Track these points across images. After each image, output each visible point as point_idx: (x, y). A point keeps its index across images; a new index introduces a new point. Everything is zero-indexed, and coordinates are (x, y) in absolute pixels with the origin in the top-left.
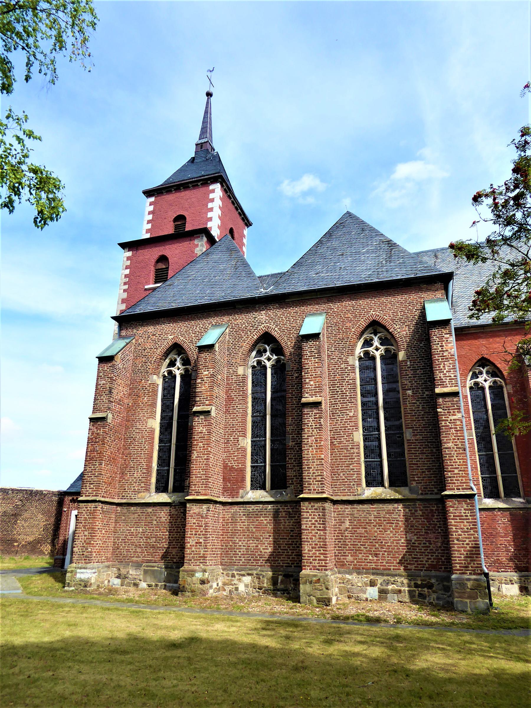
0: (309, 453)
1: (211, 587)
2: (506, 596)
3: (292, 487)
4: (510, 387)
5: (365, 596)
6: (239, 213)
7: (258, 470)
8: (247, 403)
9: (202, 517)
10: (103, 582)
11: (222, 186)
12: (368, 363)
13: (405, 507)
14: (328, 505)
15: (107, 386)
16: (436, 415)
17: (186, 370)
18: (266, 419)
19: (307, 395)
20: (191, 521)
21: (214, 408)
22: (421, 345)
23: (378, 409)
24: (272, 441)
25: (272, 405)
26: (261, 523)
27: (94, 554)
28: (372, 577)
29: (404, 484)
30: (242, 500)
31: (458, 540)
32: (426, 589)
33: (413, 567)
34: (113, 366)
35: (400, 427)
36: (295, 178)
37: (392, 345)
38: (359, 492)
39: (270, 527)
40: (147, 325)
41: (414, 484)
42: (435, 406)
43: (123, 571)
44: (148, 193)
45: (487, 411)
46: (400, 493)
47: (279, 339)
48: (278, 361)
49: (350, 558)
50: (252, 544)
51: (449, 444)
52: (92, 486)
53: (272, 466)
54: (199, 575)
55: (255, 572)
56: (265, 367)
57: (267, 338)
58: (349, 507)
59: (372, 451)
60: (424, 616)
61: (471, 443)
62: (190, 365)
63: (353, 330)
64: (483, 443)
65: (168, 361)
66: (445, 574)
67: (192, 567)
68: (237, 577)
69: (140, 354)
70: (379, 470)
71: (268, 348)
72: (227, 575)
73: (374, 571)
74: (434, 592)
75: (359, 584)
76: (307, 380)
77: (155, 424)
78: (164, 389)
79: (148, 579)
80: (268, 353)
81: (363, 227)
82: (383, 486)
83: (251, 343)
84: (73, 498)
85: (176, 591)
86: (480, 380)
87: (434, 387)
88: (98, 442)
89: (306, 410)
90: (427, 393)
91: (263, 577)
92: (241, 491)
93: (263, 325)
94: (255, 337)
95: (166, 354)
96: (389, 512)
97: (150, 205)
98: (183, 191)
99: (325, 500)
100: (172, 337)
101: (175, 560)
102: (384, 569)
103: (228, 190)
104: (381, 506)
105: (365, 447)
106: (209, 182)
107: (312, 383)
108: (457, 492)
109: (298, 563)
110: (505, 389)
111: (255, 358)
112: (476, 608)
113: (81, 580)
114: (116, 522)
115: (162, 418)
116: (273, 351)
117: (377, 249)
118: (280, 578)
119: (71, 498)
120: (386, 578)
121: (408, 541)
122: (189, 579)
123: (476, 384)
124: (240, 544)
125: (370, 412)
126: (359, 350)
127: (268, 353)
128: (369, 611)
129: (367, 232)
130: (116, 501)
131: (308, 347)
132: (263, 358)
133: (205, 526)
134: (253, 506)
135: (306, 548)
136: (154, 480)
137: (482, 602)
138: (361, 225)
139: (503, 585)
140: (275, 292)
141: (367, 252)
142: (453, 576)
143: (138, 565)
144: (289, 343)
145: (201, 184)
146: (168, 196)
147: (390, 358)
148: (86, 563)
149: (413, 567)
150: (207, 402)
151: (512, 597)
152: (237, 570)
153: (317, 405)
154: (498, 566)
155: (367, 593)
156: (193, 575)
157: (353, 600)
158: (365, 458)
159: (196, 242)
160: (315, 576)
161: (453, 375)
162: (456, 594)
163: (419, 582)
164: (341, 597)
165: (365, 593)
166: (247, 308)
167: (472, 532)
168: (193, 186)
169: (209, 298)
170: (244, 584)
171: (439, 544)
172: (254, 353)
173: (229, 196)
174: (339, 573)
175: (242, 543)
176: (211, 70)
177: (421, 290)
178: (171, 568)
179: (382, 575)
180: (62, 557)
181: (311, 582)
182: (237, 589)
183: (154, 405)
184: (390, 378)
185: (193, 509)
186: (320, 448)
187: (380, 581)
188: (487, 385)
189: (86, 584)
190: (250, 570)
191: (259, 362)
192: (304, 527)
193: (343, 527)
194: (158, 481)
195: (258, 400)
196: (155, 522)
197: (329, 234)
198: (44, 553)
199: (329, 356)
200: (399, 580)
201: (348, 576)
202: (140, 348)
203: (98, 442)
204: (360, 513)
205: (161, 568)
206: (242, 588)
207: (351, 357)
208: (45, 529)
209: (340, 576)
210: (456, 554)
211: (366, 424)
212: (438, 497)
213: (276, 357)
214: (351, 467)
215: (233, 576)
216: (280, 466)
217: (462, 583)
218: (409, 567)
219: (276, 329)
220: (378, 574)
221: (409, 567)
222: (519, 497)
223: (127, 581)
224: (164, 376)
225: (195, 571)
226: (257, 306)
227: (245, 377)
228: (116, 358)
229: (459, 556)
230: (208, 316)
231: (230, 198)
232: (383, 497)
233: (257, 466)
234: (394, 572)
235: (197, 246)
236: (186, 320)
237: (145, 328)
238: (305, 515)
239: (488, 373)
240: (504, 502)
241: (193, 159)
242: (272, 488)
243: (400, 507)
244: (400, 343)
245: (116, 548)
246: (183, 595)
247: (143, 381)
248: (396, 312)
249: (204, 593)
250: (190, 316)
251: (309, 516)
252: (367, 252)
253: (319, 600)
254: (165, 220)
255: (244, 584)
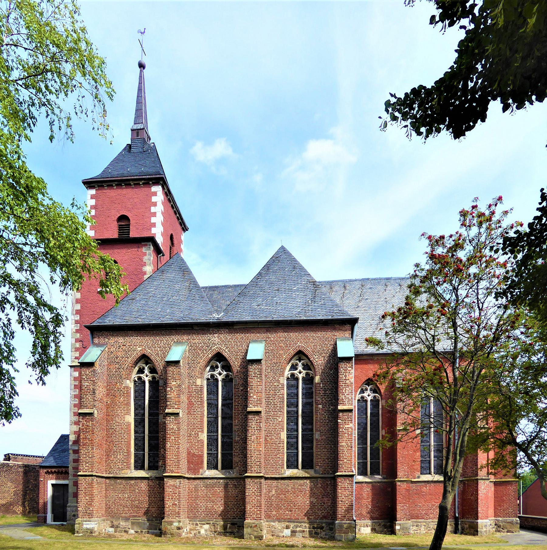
0: (252, 446)
1: (184, 531)
2: (363, 534)
3: (238, 468)
4: (384, 401)
5: (282, 534)
6: (178, 218)
7: (212, 456)
8: (204, 407)
9: (176, 488)
10: (102, 530)
11: (163, 189)
12: (293, 382)
13: (311, 482)
14: (263, 480)
15: (91, 387)
16: (337, 424)
17: (154, 378)
18: (218, 420)
19: (251, 405)
20: (168, 490)
21: (181, 411)
22: (331, 372)
23: (298, 417)
24: (223, 436)
25: (222, 409)
26: (216, 491)
27: (95, 512)
28: (287, 524)
29: (311, 467)
30: (202, 476)
31: (341, 501)
32: (319, 530)
33: (313, 517)
34: (94, 371)
35: (312, 430)
36: (209, 141)
37: (311, 370)
38: (282, 472)
39: (222, 494)
40: (117, 336)
41: (318, 467)
42: (337, 418)
43: (115, 523)
44: (89, 184)
45: (367, 417)
46: (308, 473)
47: (229, 359)
48: (227, 376)
49: (274, 513)
50: (210, 505)
51: (343, 443)
52: (87, 465)
53: (223, 454)
54: (176, 524)
55: (212, 522)
56: (217, 380)
57: (219, 357)
58: (276, 481)
59: (292, 446)
60: (318, 543)
61: (355, 439)
62: (157, 374)
63: (284, 356)
64: (362, 439)
65: (137, 368)
66: (331, 521)
67: (170, 519)
68: (199, 525)
69: (113, 360)
70: (296, 458)
71: (219, 365)
72: (193, 524)
73: (289, 520)
74: (324, 531)
75: (279, 528)
76: (252, 395)
77: (131, 419)
78: (135, 391)
79: (135, 527)
80: (219, 369)
81: (295, 265)
82: (298, 468)
83: (207, 360)
84: (48, 471)
85: (160, 533)
86: (365, 395)
87: (337, 405)
88: (89, 432)
89: (250, 417)
90: (332, 407)
91: (217, 525)
92: (201, 470)
93: (216, 346)
94: (210, 356)
95: (136, 363)
96: (301, 485)
97: (92, 198)
98: (124, 188)
99: (261, 477)
100: (140, 349)
101: (154, 516)
102: (295, 519)
103: (168, 193)
104: (296, 481)
105: (288, 443)
106: (151, 183)
107: (255, 397)
108: (344, 474)
109: (243, 515)
110: (380, 402)
111: (209, 372)
112: (347, 538)
113: (87, 529)
114: (106, 490)
115: (136, 415)
116: (223, 368)
117: (306, 288)
118: (229, 525)
119: (45, 471)
120: (296, 524)
121: (311, 502)
122: (169, 527)
123: (362, 397)
124: (201, 504)
125: (292, 418)
126: (287, 373)
127: (219, 369)
128: (286, 542)
129: (298, 270)
130: (104, 475)
131: (252, 369)
132: (216, 373)
133: (177, 493)
134: (210, 481)
135: (248, 507)
136: (132, 461)
137: (350, 535)
138: (294, 262)
139: (362, 528)
140: (225, 319)
141: (297, 290)
142: (337, 522)
143: (127, 519)
144: (236, 363)
145: (143, 184)
146: (109, 191)
147: (308, 380)
148: (90, 518)
149: (313, 517)
150: (176, 406)
151: (366, 534)
152: (199, 521)
153: (258, 413)
154: (361, 516)
155: (284, 532)
156: (172, 525)
157: (275, 537)
158: (287, 450)
159: (144, 250)
160: (254, 523)
161: (350, 397)
162: (337, 532)
163: (316, 526)
164: (267, 535)
165: (283, 533)
166: (203, 330)
167: (350, 497)
168: (135, 184)
169: (170, 317)
170: (204, 529)
171: (330, 504)
172: (208, 368)
173: (169, 200)
174: (267, 521)
175: (202, 505)
176: (143, 31)
177: (335, 329)
178: (152, 520)
179: (294, 522)
180: (44, 515)
181: (251, 527)
182: (199, 532)
183: (128, 404)
184: (308, 394)
185: (169, 482)
186: (259, 443)
187: (292, 526)
188: (369, 399)
189: (91, 531)
190: (208, 521)
191: (212, 376)
192: (247, 494)
193: (271, 494)
194: (136, 462)
195: (212, 405)
196: (137, 491)
197: (267, 267)
198: (17, 513)
199: (266, 376)
200: (304, 525)
201: (272, 523)
202: (112, 355)
203: (89, 432)
204: (282, 485)
205: (144, 520)
206: (203, 532)
207: (282, 378)
208: (16, 494)
209: (268, 523)
210: (340, 509)
211: (289, 427)
212: (332, 476)
213: (226, 373)
214: (278, 456)
215: (197, 525)
216: (228, 453)
217: (341, 526)
218: (310, 517)
219: (226, 350)
220: (291, 522)
221: (310, 517)
222: (379, 475)
223: (119, 529)
224: (135, 381)
225: (173, 522)
226: (211, 329)
227: (202, 387)
228: (95, 364)
229: (341, 510)
230: (170, 334)
231: (170, 202)
232: (298, 475)
233: (211, 453)
234: (300, 520)
235: (145, 254)
236: (153, 335)
237: (116, 339)
238: (248, 487)
239: (371, 390)
240: (369, 478)
241: (129, 147)
242: (222, 469)
243: (308, 482)
244: (317, 370)
245: (108, 508)
246: (165, 537)
247: (118, 384)
248: (315, 344)
249: (179, 535)
250: (155, 332)
251: (251, 487)
252: (297, 290)
253: (255, 537)
254: (109, 219)
255: (204, 529)
